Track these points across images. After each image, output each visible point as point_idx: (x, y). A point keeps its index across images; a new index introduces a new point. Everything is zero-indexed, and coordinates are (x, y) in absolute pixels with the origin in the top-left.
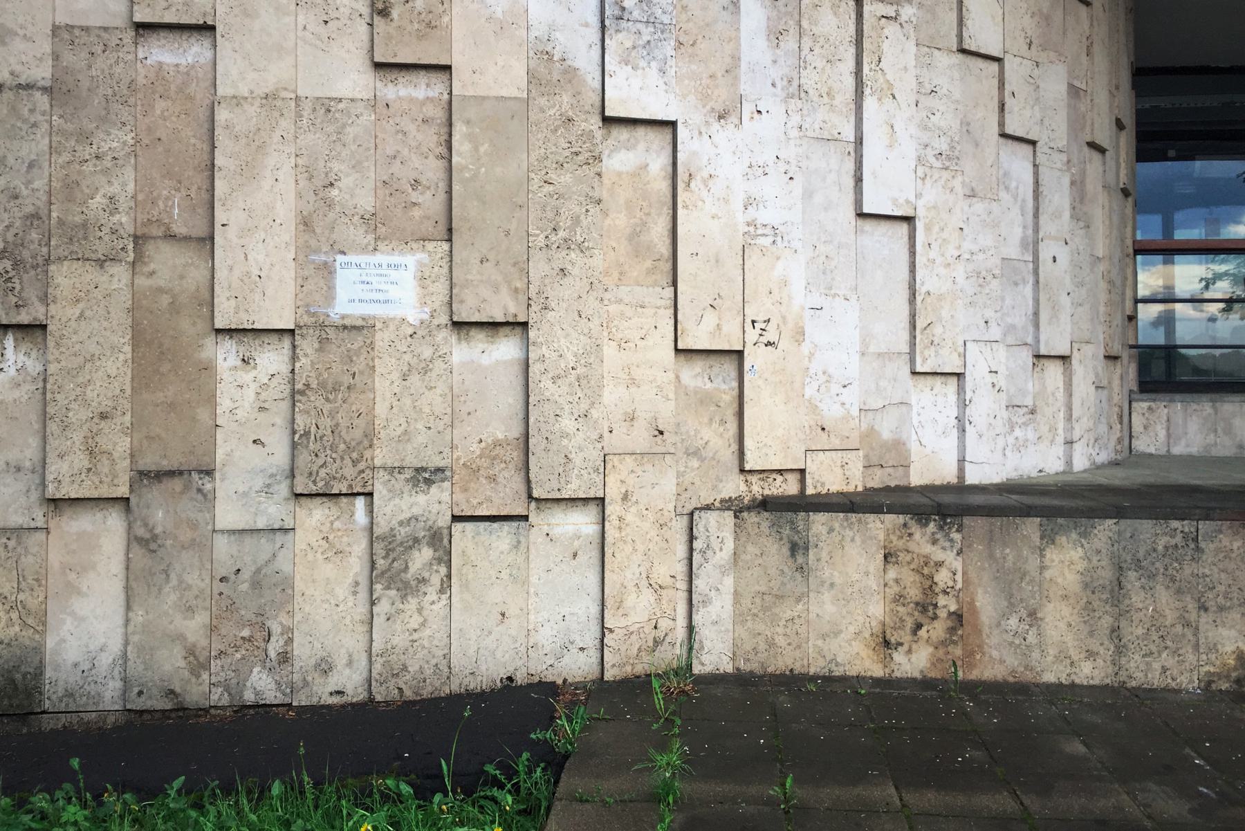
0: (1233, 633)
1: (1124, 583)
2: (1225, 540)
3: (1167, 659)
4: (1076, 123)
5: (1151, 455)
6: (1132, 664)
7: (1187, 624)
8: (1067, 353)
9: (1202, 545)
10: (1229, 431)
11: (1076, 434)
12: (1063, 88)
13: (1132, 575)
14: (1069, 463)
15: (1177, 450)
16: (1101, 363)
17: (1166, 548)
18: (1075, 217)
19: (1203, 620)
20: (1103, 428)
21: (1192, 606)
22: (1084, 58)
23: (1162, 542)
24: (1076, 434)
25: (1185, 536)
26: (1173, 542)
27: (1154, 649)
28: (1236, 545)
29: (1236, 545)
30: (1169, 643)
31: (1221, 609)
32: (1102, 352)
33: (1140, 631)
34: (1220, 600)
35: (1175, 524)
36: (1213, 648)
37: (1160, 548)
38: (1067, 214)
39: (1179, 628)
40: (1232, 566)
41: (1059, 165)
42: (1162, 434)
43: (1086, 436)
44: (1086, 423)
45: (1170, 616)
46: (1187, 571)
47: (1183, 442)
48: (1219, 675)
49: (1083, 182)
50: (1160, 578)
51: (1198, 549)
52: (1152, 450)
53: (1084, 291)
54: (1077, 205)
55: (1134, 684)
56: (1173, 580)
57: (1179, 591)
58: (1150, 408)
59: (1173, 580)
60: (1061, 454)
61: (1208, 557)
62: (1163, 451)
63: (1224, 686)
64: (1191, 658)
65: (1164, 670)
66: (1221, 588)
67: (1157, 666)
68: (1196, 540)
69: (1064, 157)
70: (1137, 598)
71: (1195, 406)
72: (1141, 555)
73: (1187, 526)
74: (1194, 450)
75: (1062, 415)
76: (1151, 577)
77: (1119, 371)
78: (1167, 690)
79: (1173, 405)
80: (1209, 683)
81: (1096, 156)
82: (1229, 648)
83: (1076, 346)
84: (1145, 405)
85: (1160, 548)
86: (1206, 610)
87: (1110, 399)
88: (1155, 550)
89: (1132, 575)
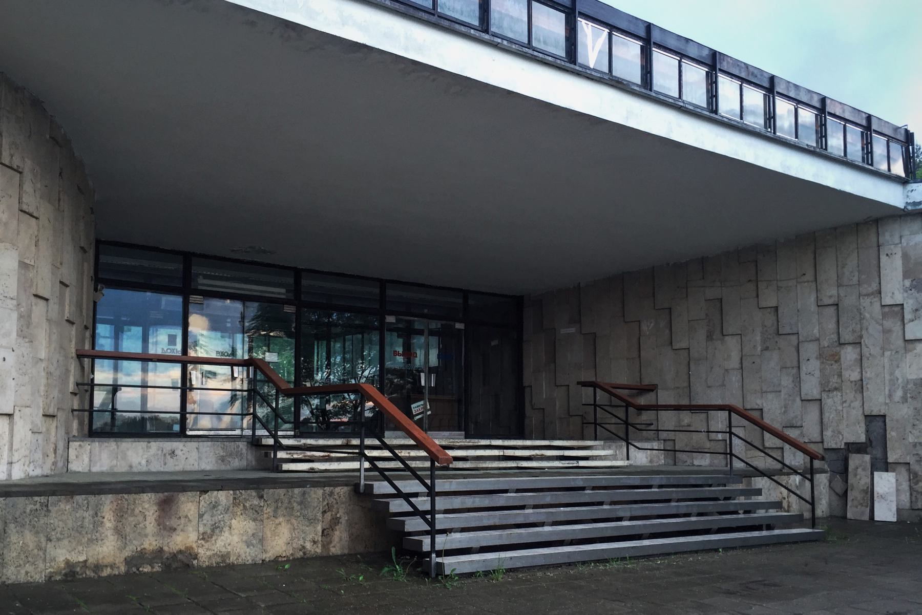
0: (64, 551)
1: (7, 530)
2: (62, 505)
3: (28, 568)
4: (25, 284)
5: (79, 472)
6: (10, 572)
7: (40, 549)
8: (11, 412)
9: (50, 508)
10: (125, 457)
11: (15, 459)
12: (16, 265)
13: (12, 526)
14: (10, 475)
15: (94, 470)
16: (39, 420)
17: (31, 511)
18: (21, 334)
19: (48, 546)
20: (39, 456)
21: (43, 539)
22: (33, 248)
23: (30, 507)
24: (15, 459)
25: (41, 504)
26: (35, 508)
27: (21, 562)
28: (68, 507)
29: (68, 507)
30: (30, 559)
31: (59, 540)
32: (41, 412)
33: (15, 554)
34: (58, 535)
35: (36, 498)
36: (54, 559)
37: (28, 511)
38: (14, 335)
39: (36, 551)
40: (64, 517)
41: (11, 306)
42: (86, 460)
43: (23, 460)
44: (23, 452)
45: (32, 546)
46: (42, 522)
47: (98, 464)
48: (56, 573)
49: (29, 316)
50: (27, 526)
51: (49, 511)
52: (80, 469)
53: (26, 378)
54: (24, 328)
55: (10, 582)
56: (34, 527)
57: (37, 532)
58: (80, 446)
59: (34, 527)
60: (5, 470)
61: (53, 514)
62: (86, 470)
63: (58, 578)
64: (41, 566)
65: (27, 573)
66: (59, 530)
67: (23, 572)
68: (47, 506)
69: (15, 302)
70: (14, 538)
71: (106, 444)
72: (17, 516)
73: (43, 499)
74: (104, 469)
75: (6, 447)
76: (23, 526)
77: (54, 424)
78: (28, 583)
79: (93, 444)
80: (50, 577)
81: (42, 303)
82: (62, 559)
83: (17, 409)
84: (77, 444)
85: (28, 511)
86: (51, 541)
87: (47, 440)
88: (25, 512)
89: (12, 526)
